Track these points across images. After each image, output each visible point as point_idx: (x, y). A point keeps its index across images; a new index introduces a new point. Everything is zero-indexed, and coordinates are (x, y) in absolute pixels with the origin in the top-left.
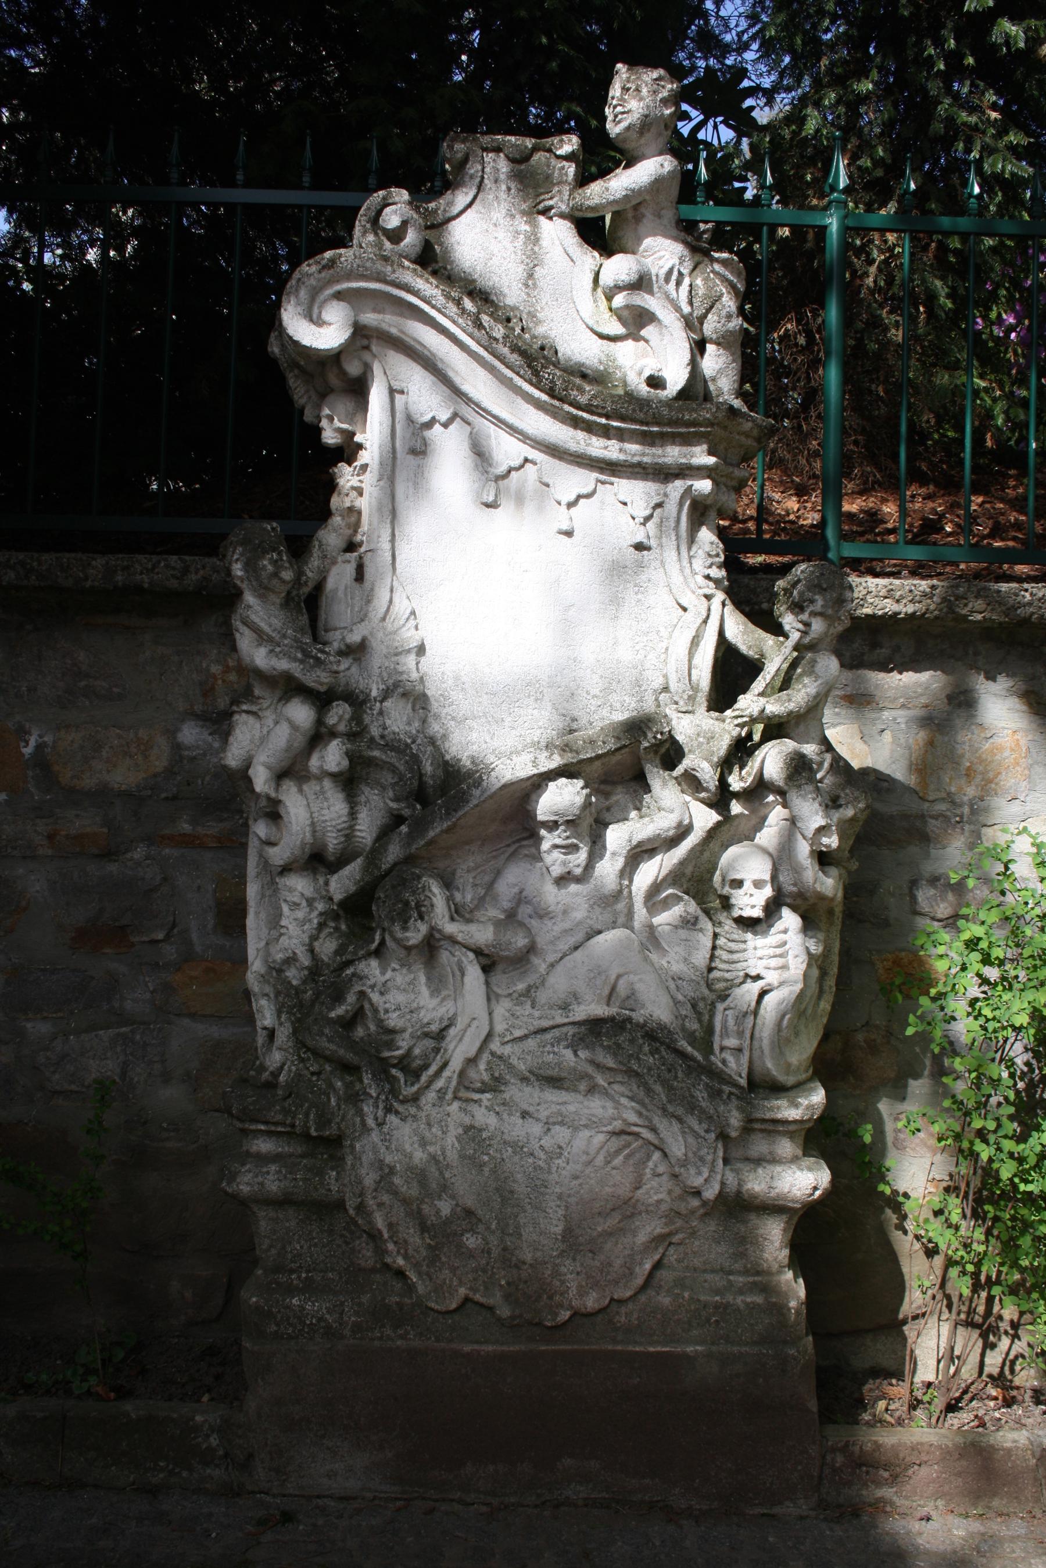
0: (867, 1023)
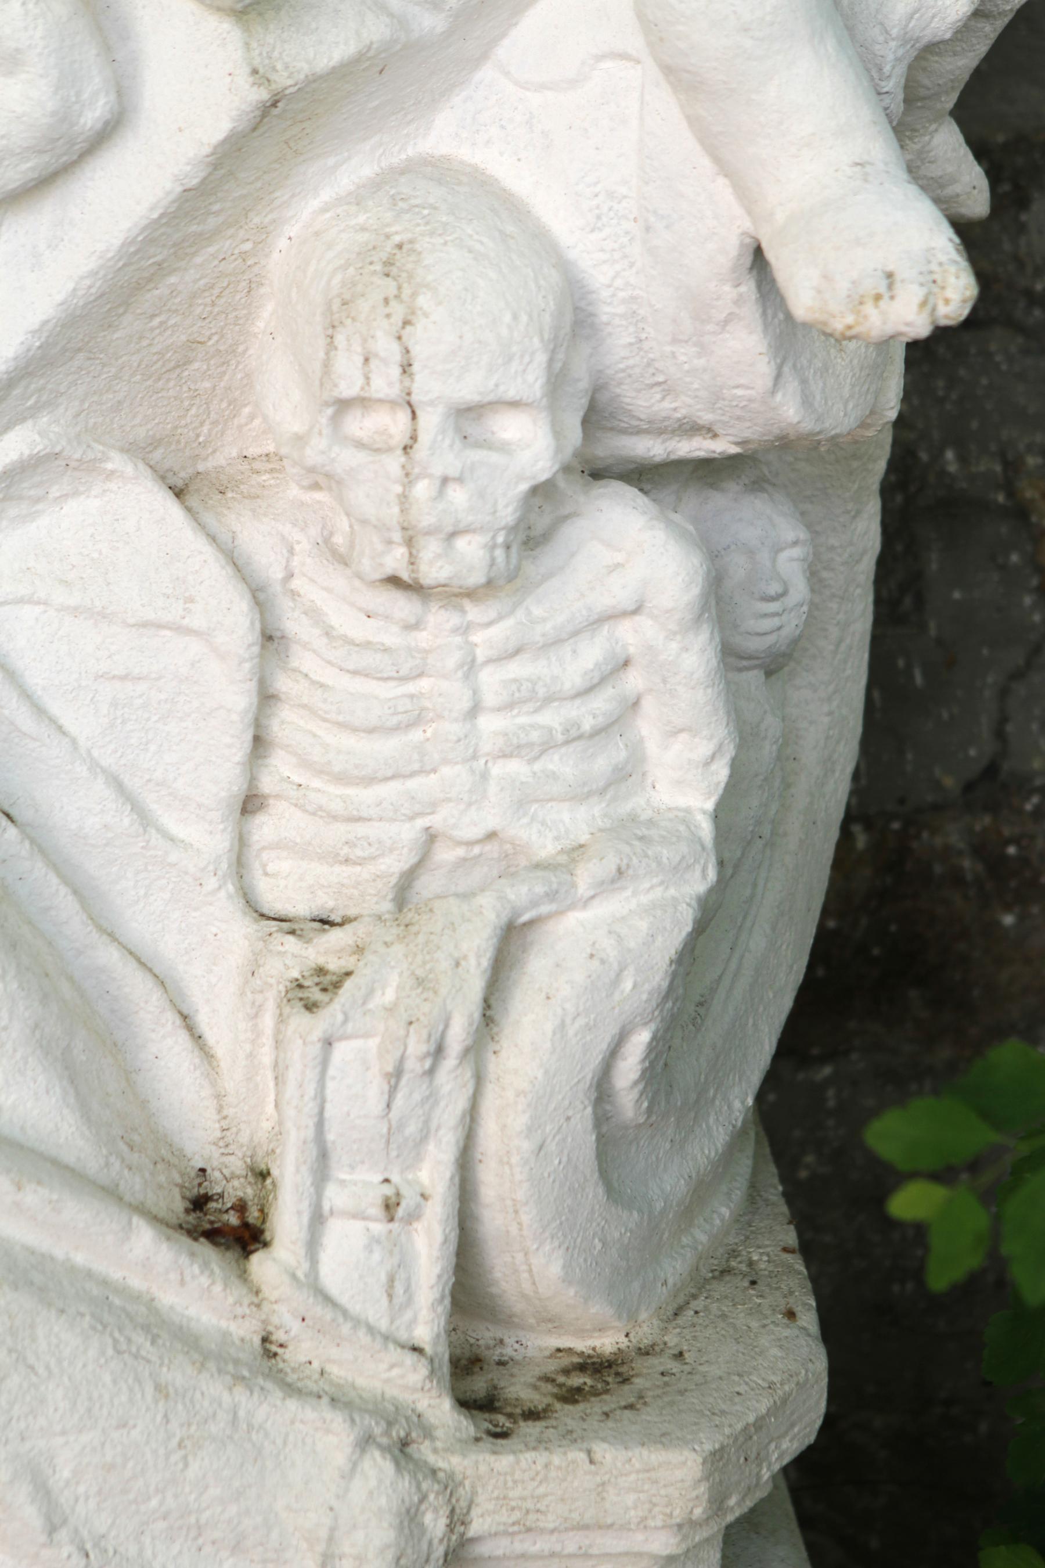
0: (991, 771)
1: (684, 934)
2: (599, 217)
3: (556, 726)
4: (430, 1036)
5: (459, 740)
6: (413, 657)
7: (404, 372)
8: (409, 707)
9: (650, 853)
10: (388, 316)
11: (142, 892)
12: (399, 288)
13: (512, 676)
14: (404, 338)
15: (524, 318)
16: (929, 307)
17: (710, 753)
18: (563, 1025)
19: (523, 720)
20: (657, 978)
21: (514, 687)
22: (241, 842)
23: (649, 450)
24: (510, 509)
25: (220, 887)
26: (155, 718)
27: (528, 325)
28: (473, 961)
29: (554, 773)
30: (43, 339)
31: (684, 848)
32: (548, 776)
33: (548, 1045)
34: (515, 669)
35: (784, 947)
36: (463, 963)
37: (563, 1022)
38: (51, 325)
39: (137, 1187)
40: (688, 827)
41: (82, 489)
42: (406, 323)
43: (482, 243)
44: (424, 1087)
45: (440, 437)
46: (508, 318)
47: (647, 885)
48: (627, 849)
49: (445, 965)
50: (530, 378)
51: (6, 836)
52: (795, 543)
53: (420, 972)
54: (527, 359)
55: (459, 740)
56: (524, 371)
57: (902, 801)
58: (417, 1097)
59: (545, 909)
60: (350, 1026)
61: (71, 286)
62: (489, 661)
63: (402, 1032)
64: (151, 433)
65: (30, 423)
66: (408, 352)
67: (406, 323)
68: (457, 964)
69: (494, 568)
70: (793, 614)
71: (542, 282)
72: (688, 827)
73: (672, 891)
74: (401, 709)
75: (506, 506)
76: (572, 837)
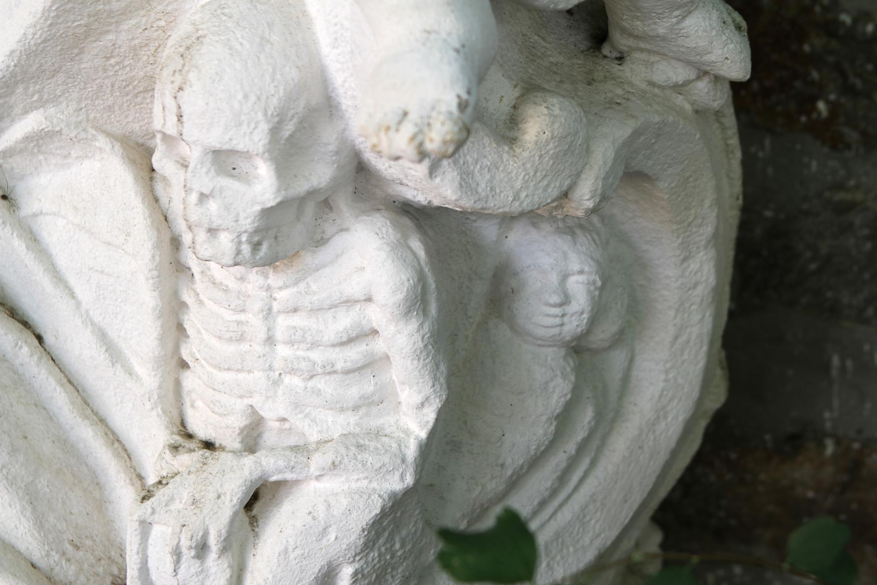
1: (373, 514)
2: (336, 39)
3: (319, 361)
4: (192, 537)
5: (260, 357)
6: (239, 298)
7: (179, 120)
8: (236, 329)
9: (359, 457)
10: (173, 82)
11: (119, 400)
12: (184, 65)
13: (295, 324)
14: (178, 98)
15: (253, 98)
16: (416, 142)
17: (419, 401)
18: (286, 551)
19: (300, 353)
20: (353, 538)
21: (292, 332)
22: (178, 384)
23: (414, 197)
24: (249, 221)
25: (152, 409)
26: (120, 300)
27: (255, 103)
28: (228, 498)
29: (320, 391)
30: (16, 62)
31: (386, 459)
32: (313, 392)
33: (276, 560)
34: (297, 320)
35: (593, 522)
36: (223, 497)
37: (286, 549)
38: (17, 53)
39: (71, 572)
40: (400, 446)
41: (90, 155)
42: (181, 89)
43: (241, 44)
44: (197, 565)
45: (199, 166)
46: (240, 96)
47: (356, 477)
48: (343, 451)
49: (212, 495)
50: (256, 138)
51: (22, 351)
52: (581, 272)
53: (197, 496)
54: (252, 126)
55: (260, 357)
56: (251, 133)
57: (860, 432)
58: (193, 570)
59: (289, 476)
60: (156, 517)
61: (22, 31)
62: (279, 312)
63: (178, 530)
64: (144, 128)
65: (42, 110)
66: (180, 108)
67: (181, 89)
68: (219, 497)
69: (240, 256)
70: (574, 318)
71: (278, 76)
72: (400, 446)
73: (374, 485)
74: (231, 329)
75: (246, 218)
76: (330, 433)
